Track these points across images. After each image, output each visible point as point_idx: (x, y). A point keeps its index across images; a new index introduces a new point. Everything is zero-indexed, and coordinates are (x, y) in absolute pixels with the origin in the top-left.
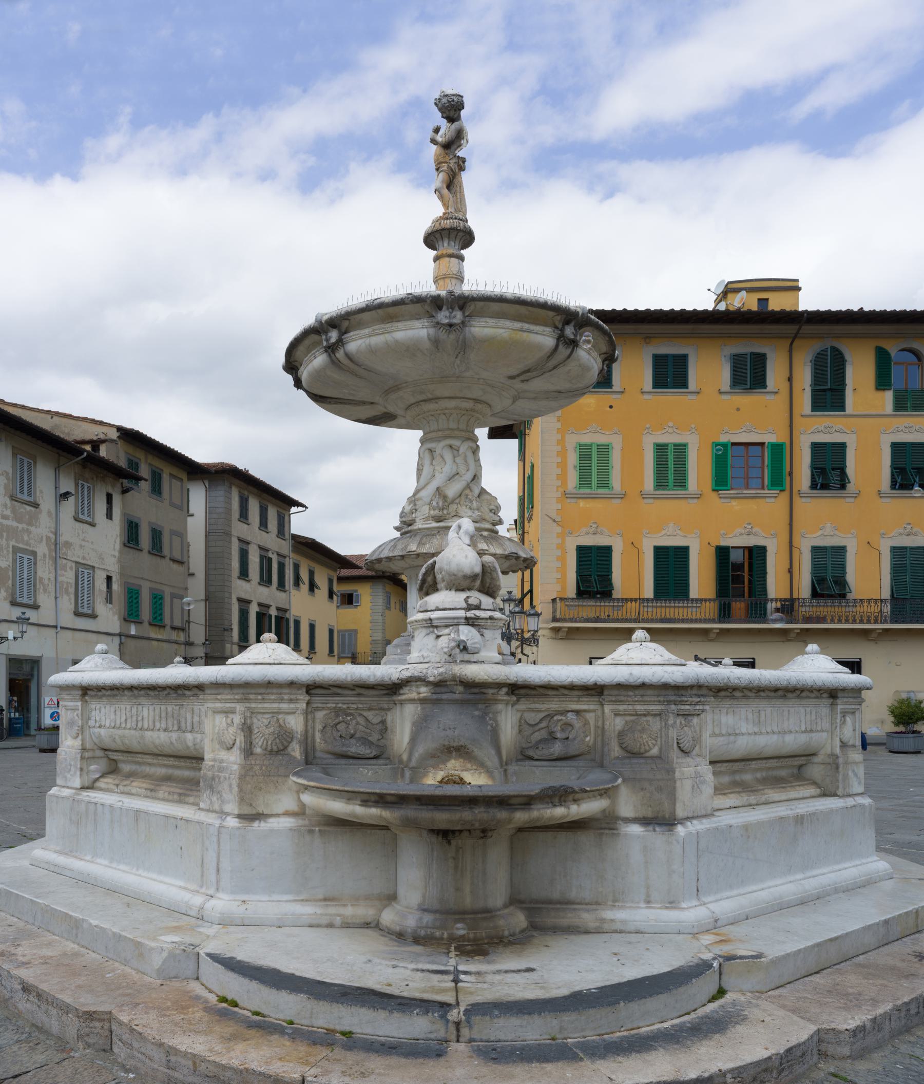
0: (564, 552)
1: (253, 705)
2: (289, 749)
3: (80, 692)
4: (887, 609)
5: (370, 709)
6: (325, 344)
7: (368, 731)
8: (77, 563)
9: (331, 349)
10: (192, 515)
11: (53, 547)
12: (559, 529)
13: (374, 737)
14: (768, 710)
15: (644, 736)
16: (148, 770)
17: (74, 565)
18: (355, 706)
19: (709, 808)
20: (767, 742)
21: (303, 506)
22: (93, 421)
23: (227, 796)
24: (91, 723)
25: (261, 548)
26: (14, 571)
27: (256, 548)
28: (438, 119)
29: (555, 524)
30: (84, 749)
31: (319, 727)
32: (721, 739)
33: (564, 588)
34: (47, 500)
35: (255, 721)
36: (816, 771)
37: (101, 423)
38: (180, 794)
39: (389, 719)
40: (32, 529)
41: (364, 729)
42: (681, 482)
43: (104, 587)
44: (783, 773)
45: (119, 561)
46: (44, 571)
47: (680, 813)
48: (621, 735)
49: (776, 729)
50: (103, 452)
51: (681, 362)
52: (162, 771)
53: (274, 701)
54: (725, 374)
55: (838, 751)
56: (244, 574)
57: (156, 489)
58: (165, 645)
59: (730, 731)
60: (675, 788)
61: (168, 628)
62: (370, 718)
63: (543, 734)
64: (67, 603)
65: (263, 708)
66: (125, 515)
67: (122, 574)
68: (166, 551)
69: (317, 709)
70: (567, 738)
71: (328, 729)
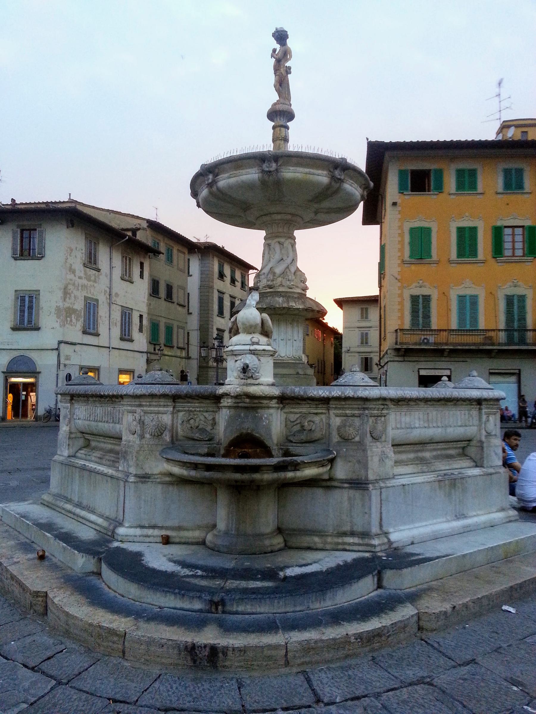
1: (145, 408)
2: (164, 435)
3: (69, 398)
5: (207, 411)
6: (206, 183)
7: (205, 424)
9: (210, 185)
10: (191, 276)
11: (108, 297)
12: (399, 284)
13: (209, 428)
14: (434, 413)
15: (351, 429)
16: (102, 445)
17: (120, 307)
18: (198, 409)
19: (391, 474)
20: (434, 432)
22: (133, 216)
23: (131, 463)
24: (75, 417)
25: (231, 296)
27: (228, 296)
29: (397, 281)
30: (71, 433)
31: (180, 422)
32: (402, 431)
33: (403, 323)
35: (146, 418)
36: (472, 451)
37: (138, 217)
38: (113, 461)
39: (217, 417)
40: (95, 285)
41: (203, 423)
42: (474, 253)
44: (452, 452)
47: (371, 477)
48: (339, 429)
49: (439, 424)
50: (140, 236)
51: (473, 173)
52: (109, 446)
53: (156, 406)
55: (483, 439)
56: (221, 313)
57: (170, 259)
58: (174, 359)
59: (407, 426)
60: (367, 460)
61: (175, 347)
62: (207, 416)
63: (297, 428)
64: (116, 332)
65: (150, 410)
66: (150, 275)
68: (175, 299)
69: (179, 411)
70: (311, 430)
71: (185, 423)
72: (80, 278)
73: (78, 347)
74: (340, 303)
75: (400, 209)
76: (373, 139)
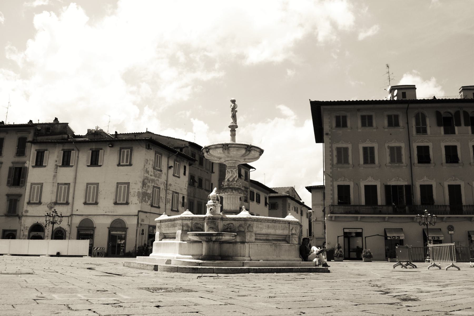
0: (333, 188)
4: (448, 209)
8: (173, 191)
21: (254, 168)
26: (153, 194)
28: (231, 103)
33: (334, 201)
34: (164, 169)
40: (159, 179)
43: (181, 201)
45: (187, 191)
46: (163, 195)
51: (370, 118)
54: (386, 122)
66: (190, 173)
67: (188, 196)
68: (203, 187)
72: (151, 175)
73: (148, 215)
74: (310, 189)
75: (330, 137)
76: (313, 100)
